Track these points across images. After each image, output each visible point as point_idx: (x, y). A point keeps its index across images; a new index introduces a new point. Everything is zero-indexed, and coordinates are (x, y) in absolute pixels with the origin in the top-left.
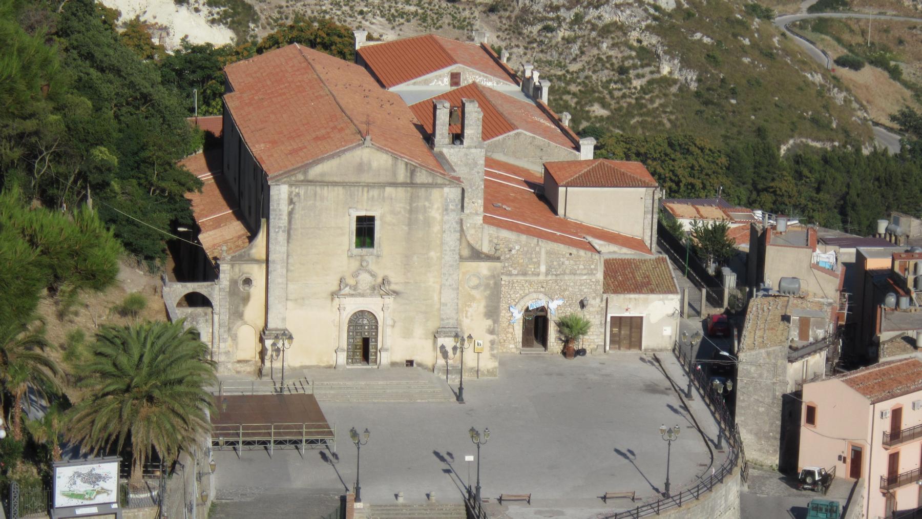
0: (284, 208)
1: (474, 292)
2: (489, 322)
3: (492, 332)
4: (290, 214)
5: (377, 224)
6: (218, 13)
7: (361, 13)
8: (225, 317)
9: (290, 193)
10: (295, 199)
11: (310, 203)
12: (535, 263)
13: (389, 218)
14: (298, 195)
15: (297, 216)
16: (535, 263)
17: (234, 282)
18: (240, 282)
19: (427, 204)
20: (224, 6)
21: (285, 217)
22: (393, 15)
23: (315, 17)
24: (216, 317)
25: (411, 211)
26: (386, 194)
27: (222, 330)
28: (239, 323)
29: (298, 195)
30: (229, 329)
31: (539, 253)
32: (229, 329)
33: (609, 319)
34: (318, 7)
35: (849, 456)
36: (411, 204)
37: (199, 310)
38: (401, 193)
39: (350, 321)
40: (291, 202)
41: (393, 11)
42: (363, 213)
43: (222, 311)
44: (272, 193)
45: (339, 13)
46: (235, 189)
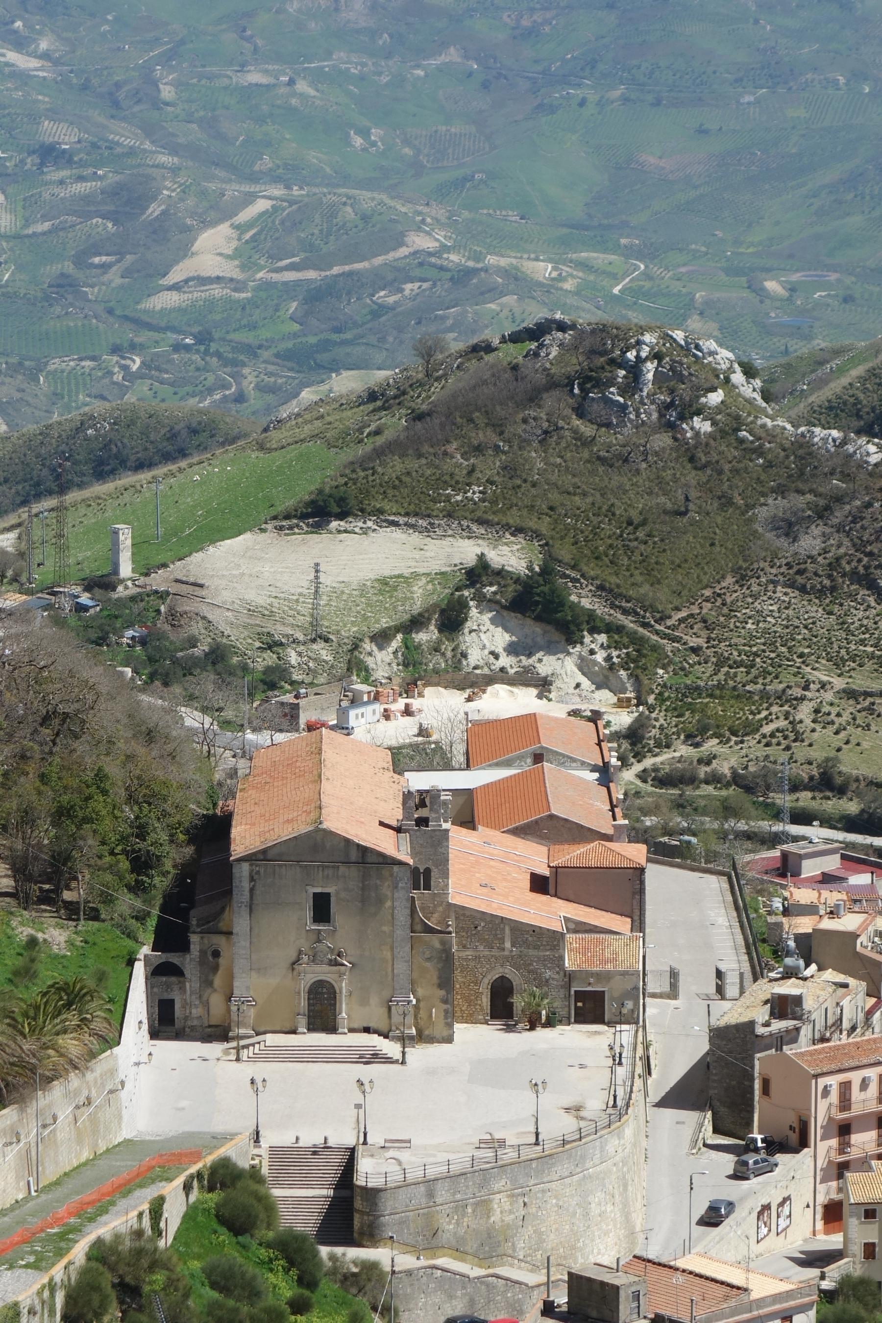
0: (246, 885)
1: (428, 964)
2: (442, 993)
3: (445, 1002)
4: (252, 890)
5: (333, 899)
6: (618, 657)
7: (801, 656)
8: (196, 985)
9: (251, 872)
10: (256, 877)
11: (269, 880)
12: (499, 939)
13: (343, 895)
14: (258, 872)
15: (257, 892)
16: (499, 939)
17: (203, 953)
18: (209, 953)
19: (378, 882)
20: (627, 648)
21: (247, 893)
22: (842, 658)
23: (742, 660)
24: (188, 985)
25: (363, 889)
26: (340, 873)
27: (194, 997)
28: (209, 991)
29: (258, 872)
30: (200, 997)
31: (504, 929)
32: (200, 997)
33: (572, 993)
34: (747, 648)
35: (796, 1125)
36: (363, 882)
37: (173, 979)
38: (353, 872)
39: (310, 992)
40: (252, 879)
41: (843, 652)
42: (319, 890)
43: (193, 979)
44: (234, 871)
45: (773, 655)
46: (837, 845)
